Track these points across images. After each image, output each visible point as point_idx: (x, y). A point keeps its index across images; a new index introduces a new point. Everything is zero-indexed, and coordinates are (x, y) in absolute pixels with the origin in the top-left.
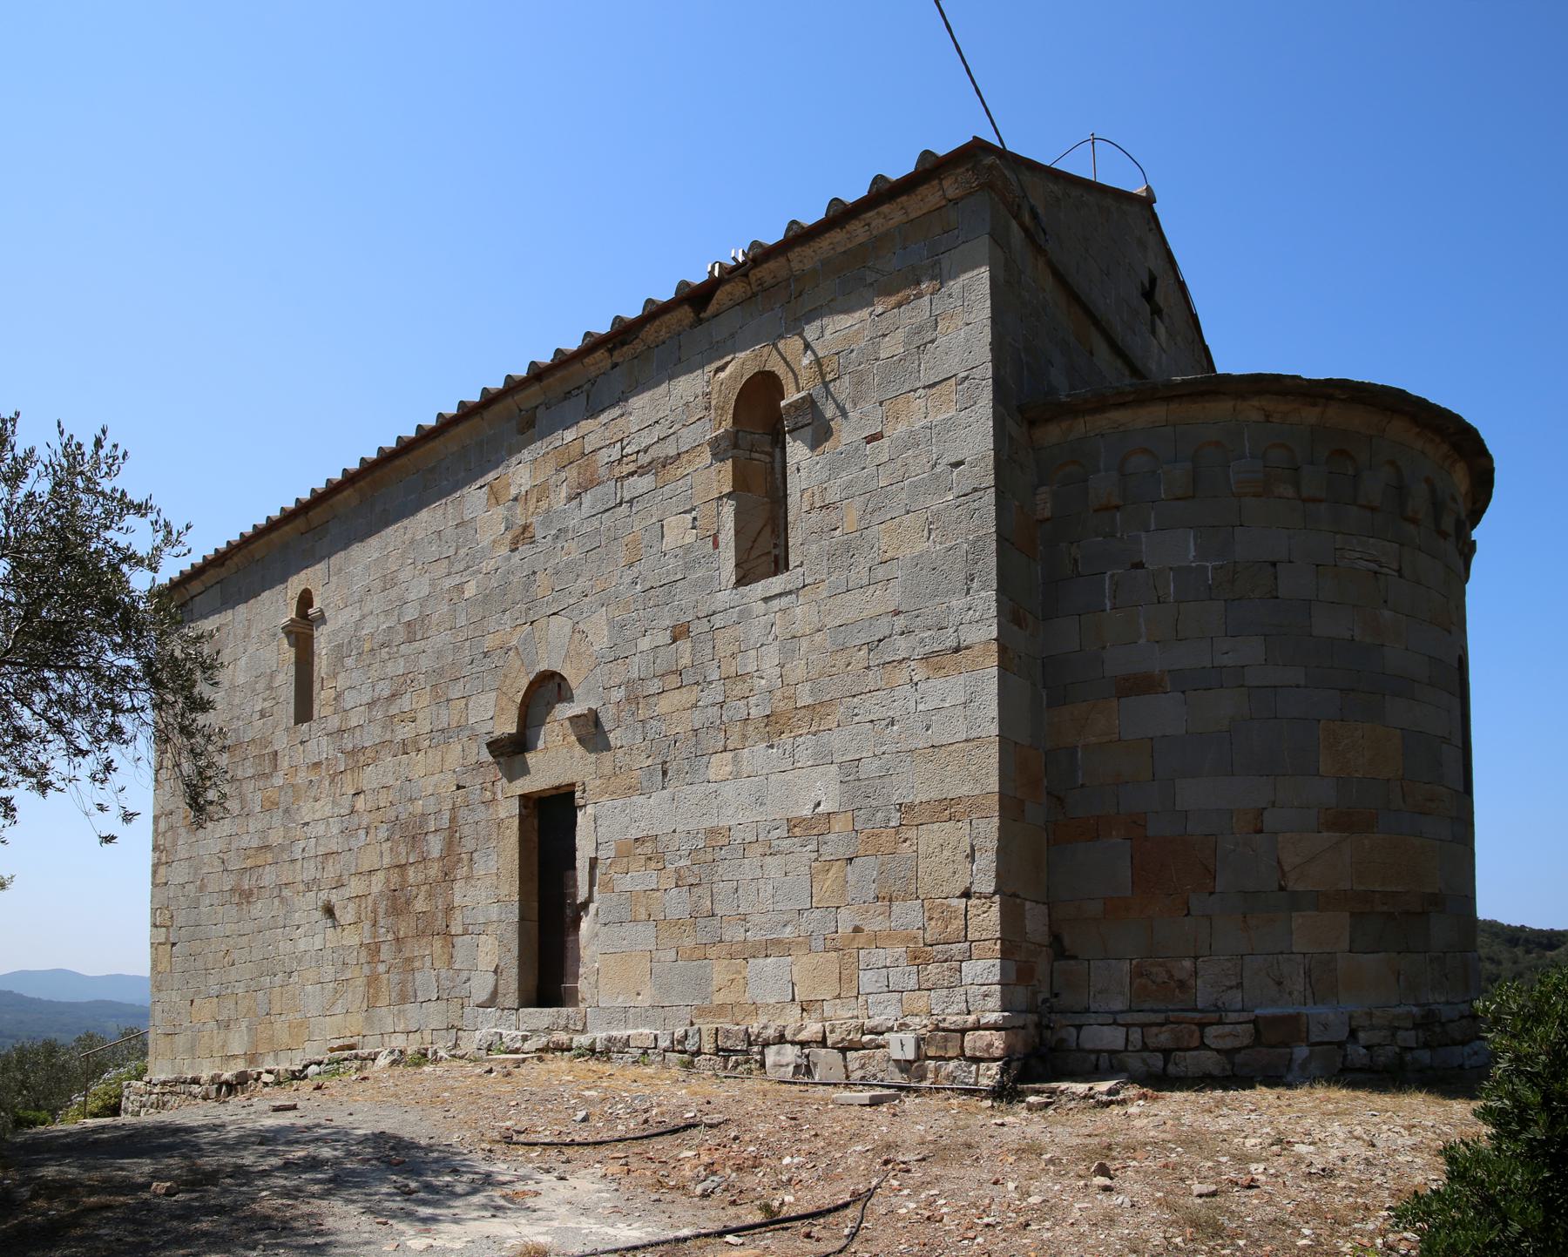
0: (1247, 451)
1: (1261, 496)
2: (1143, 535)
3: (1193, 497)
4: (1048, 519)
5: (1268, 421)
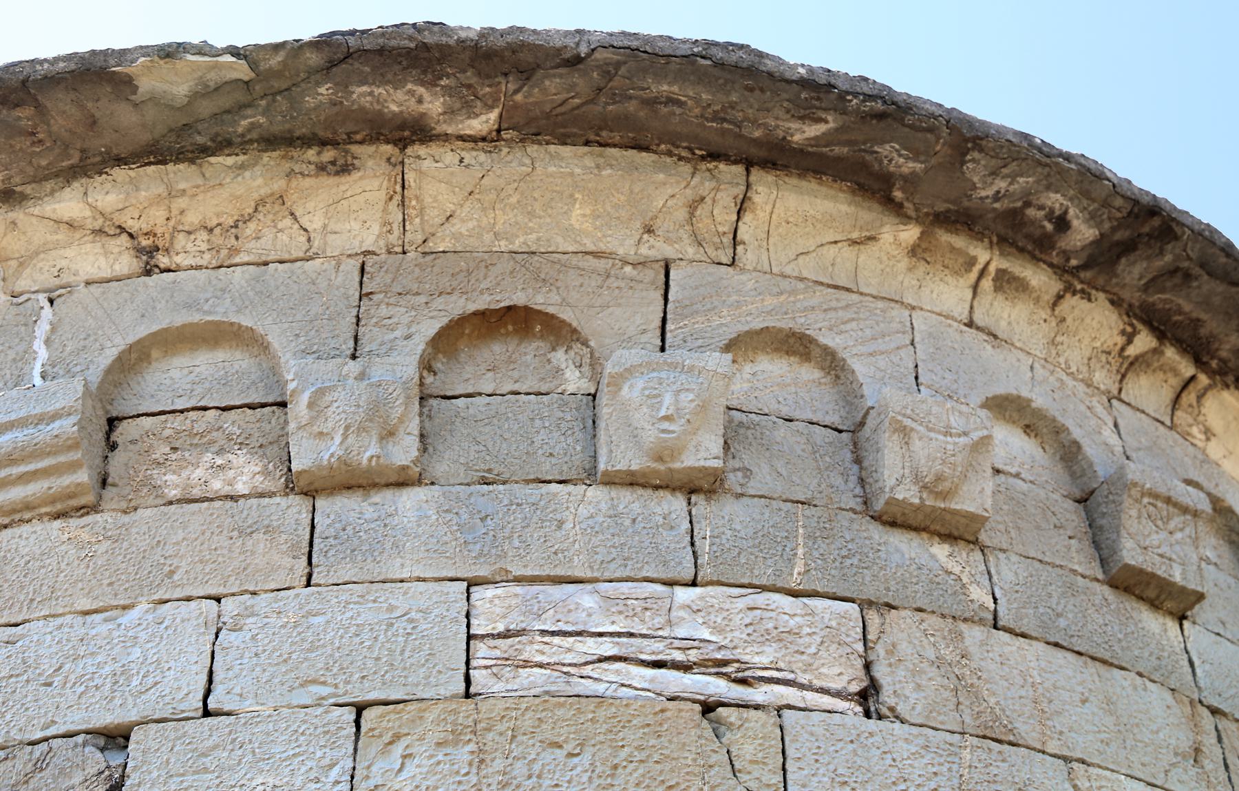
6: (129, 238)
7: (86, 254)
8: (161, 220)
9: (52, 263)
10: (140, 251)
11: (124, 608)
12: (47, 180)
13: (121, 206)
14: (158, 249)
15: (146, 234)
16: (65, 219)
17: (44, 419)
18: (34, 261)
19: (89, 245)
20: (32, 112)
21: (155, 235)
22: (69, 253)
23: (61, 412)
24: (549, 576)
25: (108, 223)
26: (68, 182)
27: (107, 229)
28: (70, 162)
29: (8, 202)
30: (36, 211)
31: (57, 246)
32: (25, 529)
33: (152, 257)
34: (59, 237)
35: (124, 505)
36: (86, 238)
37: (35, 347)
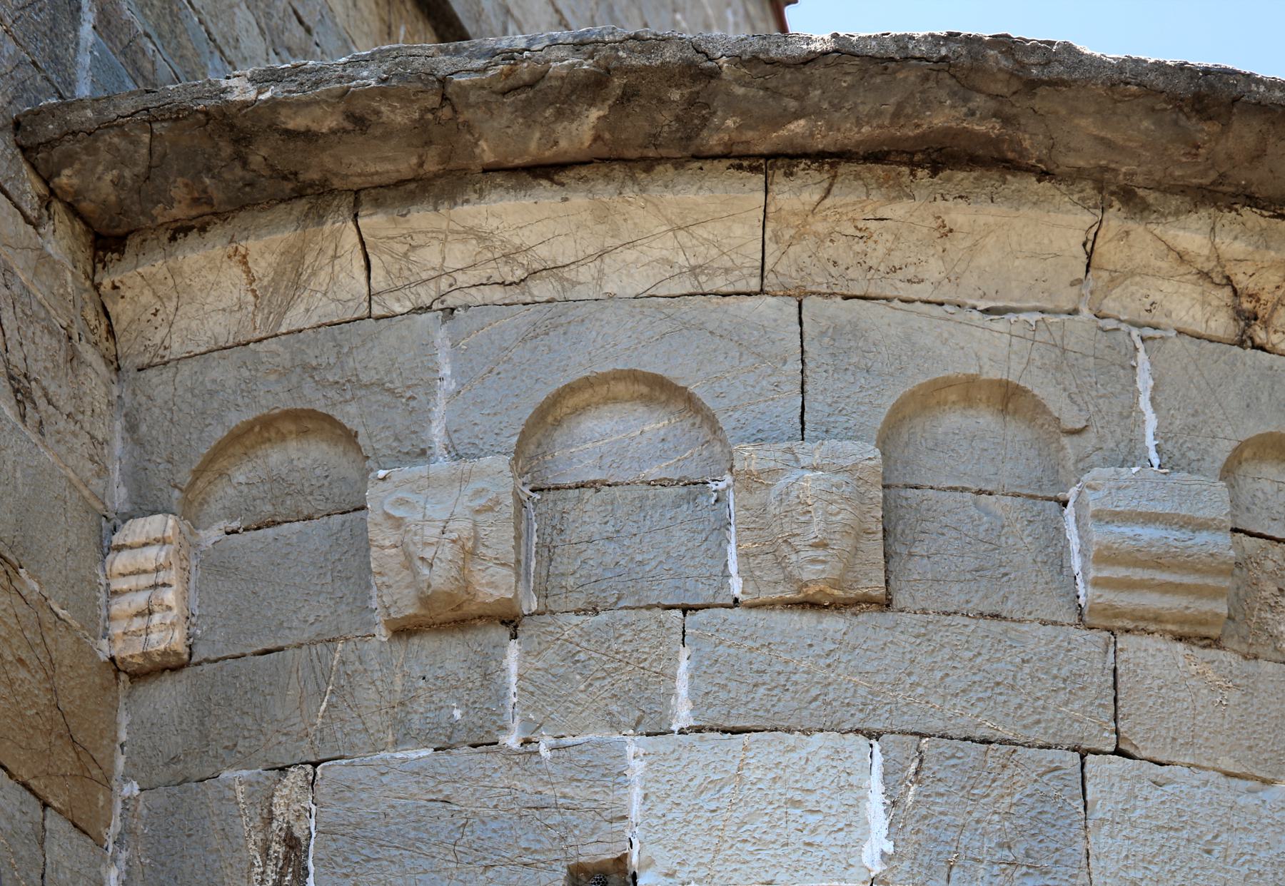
0: (1150, 442)
1: (1213, 642)
2: (634, 746)
3: (885, 604)
4: (169, 666)
5: (1245, 341)
6: (1231, 294)
7: (1184, 295)
8: (1270, 287)
9: (1145, 291)
10: (1239, 314)
11: (1264, 781)
12: (1172, 194)
13: (1242, 257)
14: (1256, 319)
15: (1250, 296)
16: (1179, 248)
17: (1190, 524)
18: (1128, 282)
19: (1190, 286)
20: (1218, 130)
21: (1258, 300)
22: (1167, 286)
23: (1210, 523)
24: (616, 371)
25: (1219, 269)
26: (1196, 206)
27: (1214, 275)
28: (1200, 181)
29: (1128, 205)
30: (1158, 230)
31: (1157, 274)
32: (1147, 641)
33: (1249, 326)
34: (1164, 265)
35: (1244, 648)
36: (1189, 277)
37: (1142, 405)
